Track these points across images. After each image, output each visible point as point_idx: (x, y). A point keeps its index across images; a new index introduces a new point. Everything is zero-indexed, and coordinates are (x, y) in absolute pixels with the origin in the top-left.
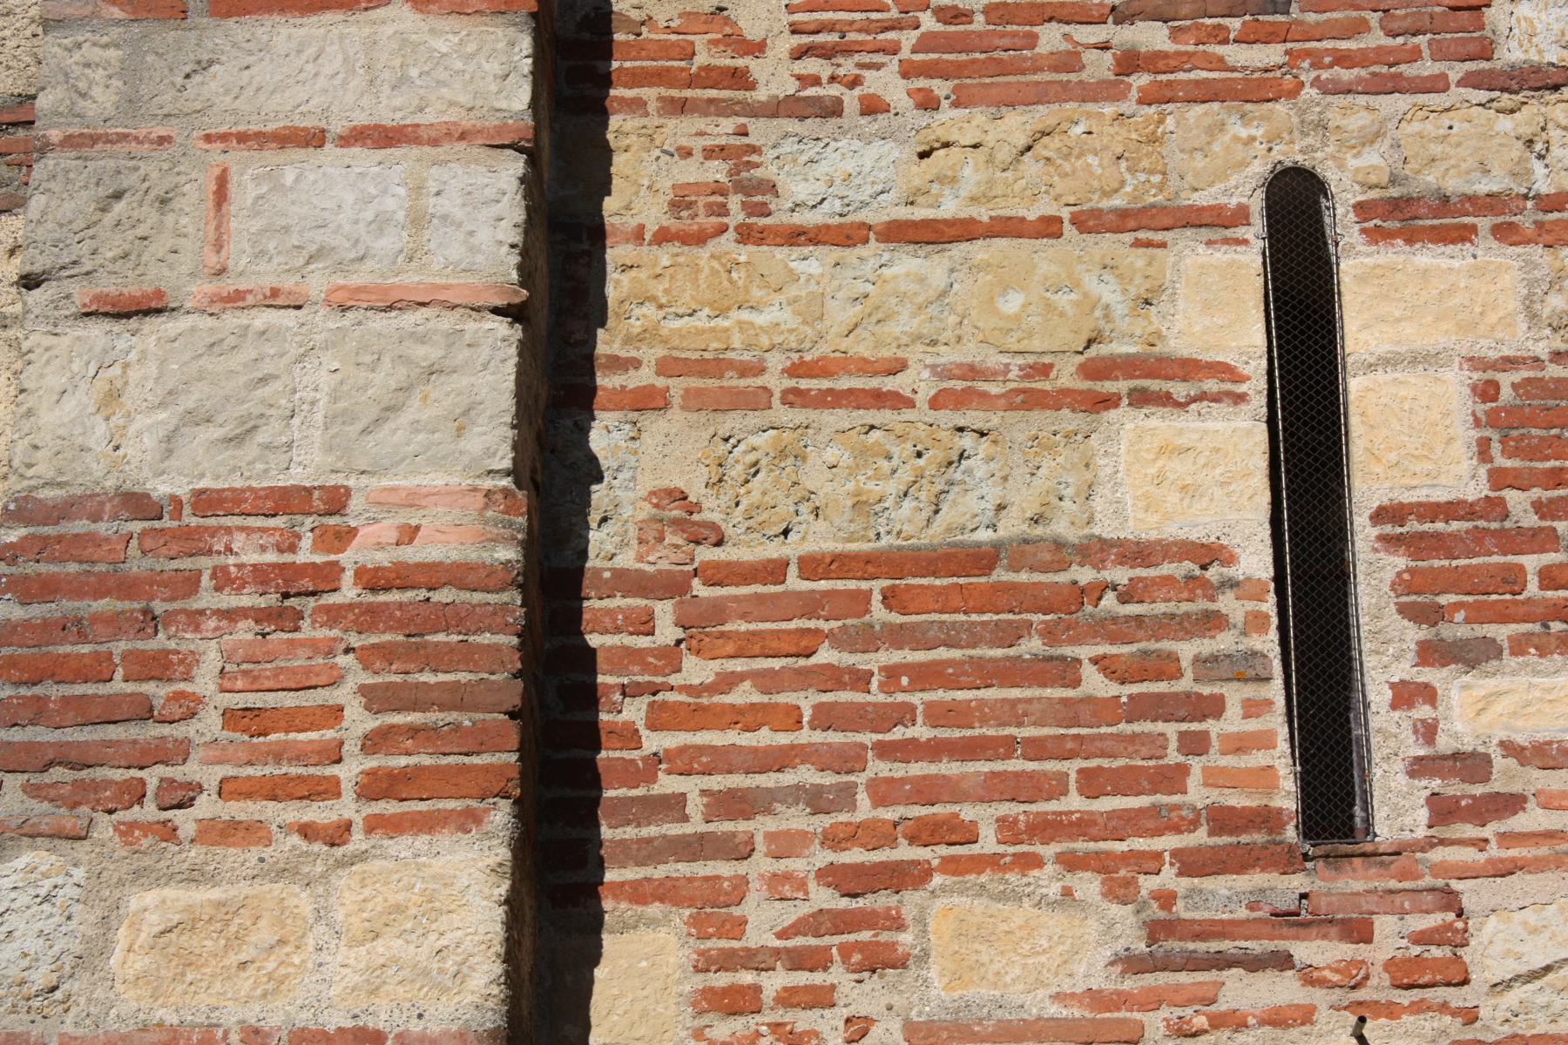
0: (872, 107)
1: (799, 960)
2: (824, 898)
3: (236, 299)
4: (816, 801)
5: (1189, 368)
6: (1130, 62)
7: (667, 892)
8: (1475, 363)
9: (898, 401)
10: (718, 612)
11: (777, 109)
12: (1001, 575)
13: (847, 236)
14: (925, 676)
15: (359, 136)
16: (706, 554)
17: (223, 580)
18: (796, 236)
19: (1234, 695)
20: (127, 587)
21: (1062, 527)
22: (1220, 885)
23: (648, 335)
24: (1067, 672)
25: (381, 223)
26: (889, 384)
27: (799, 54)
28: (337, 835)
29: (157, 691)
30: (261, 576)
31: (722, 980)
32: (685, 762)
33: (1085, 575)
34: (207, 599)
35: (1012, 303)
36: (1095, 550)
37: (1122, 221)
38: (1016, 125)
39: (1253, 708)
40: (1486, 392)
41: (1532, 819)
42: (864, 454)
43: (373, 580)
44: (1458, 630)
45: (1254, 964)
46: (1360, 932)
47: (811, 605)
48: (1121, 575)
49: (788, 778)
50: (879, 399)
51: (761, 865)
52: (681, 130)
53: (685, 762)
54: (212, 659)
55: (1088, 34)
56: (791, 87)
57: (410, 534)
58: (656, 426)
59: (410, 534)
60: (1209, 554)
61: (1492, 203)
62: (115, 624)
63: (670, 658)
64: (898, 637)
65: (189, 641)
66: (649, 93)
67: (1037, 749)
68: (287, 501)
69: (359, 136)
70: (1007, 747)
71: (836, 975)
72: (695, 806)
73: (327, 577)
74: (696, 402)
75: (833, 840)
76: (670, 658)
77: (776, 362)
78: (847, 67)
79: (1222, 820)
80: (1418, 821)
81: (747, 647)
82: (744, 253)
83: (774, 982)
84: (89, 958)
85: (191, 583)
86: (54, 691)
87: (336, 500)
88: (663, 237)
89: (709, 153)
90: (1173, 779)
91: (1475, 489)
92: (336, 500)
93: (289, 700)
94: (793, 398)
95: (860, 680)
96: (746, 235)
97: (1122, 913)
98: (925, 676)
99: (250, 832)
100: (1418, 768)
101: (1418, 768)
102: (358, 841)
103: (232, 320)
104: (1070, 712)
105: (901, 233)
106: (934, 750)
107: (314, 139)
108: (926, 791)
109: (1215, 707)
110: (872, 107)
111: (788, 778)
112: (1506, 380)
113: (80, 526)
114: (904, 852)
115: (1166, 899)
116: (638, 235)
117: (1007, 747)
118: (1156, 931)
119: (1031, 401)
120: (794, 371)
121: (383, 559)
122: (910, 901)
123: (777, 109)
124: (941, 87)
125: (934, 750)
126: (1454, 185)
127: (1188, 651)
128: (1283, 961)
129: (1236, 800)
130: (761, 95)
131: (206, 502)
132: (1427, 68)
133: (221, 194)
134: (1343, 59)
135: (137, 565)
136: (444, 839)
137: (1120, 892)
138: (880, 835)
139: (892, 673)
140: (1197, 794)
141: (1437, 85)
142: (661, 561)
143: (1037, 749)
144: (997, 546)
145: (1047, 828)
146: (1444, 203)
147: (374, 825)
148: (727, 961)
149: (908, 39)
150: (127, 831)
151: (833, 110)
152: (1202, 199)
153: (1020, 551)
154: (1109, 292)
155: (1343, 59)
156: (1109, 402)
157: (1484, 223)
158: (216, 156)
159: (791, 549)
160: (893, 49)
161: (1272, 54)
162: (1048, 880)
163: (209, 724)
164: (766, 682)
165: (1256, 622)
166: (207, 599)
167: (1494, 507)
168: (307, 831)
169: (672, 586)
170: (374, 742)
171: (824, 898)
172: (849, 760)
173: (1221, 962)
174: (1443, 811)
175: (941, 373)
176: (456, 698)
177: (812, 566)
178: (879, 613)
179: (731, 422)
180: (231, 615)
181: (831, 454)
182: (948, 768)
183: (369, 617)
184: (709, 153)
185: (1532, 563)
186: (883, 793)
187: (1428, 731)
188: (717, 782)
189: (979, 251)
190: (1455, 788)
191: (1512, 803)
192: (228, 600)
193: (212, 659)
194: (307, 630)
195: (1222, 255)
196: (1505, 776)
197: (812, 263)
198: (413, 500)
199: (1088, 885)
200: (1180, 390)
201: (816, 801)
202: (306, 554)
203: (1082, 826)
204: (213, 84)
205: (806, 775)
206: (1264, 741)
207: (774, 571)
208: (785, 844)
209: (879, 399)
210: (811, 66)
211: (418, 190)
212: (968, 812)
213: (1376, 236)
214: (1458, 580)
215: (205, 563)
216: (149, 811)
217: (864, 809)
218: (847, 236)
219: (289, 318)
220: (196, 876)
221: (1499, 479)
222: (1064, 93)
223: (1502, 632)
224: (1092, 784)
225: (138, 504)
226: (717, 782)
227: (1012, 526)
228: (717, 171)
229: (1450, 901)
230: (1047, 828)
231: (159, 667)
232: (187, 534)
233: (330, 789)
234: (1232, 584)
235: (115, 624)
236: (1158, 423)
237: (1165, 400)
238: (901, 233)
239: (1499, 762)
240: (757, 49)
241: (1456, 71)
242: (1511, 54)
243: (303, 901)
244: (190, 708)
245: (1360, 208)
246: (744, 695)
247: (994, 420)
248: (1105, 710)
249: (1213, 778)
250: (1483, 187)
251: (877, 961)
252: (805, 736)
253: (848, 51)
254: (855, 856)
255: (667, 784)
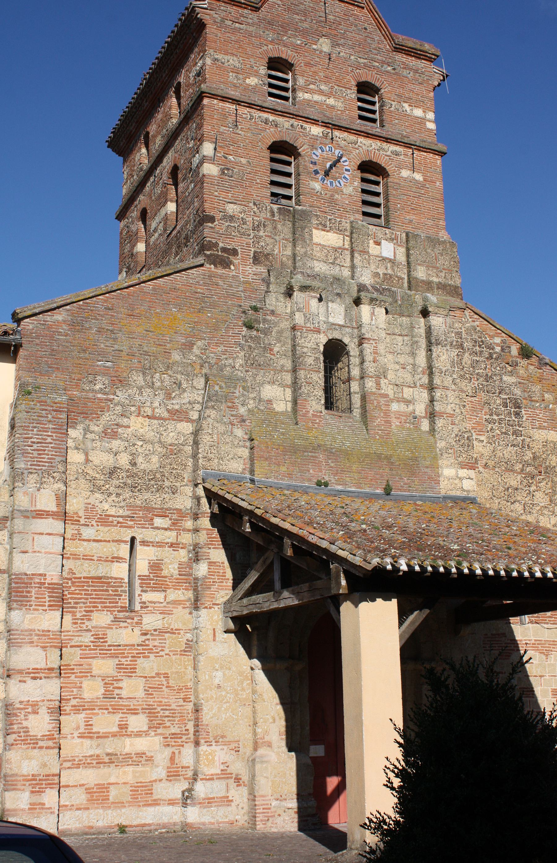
0: (92, 526)
1: (82, 619)
2: (84, 613)
3: (35, 552)
4: (84, 603)
5: (122, 558)
6: (118, 523)
7: (70, 612)
8: (149, 560)
9: (94, 560)
10: (75, 582)
11: (83, 525)
12: (102, 580)
13: (89, 541)
14: (95, 590)
15: (47, 534)
16: (74, 576)
17: (34, 583)
18: (84, 540)
19: (124, 594)
20: (25, 583)
21: (108, 575)
22: (121, 614)
23: (69, 550)
24: (108, 591)
25: (49, 544)
26: (92, 558)
27: (85, 518)
28: (46, 610)
29: (28, 595)
30: (38, 583)
31: (74, 621)
32: (71, 598)
33: (110, 580)
34: (33, 585)
35: (105, 550)
36: (111, 578)
37: (117, 541)
38: (107, 529)
39: (125, 596)
40: (150, 563)
41: (149, 609)
42: (90, 565)
43: (49, 584)
44: (145, 589)
45: (123, 622)
46: (133, 619)
47: (84, 582)
48: (114, 581)
49: (81, 601)
50: (91, 560)
51: (78, 609)
52: (73, 526)
53: (71, 598)
54: (33, 592)
55: (114, 519)
56: (84, 523)
57: (52, 579)
58: (69, 561)
59: (52, 579)
60: (122, 579)
61: (152, 542)
62: (24, 587)
63: (70, 587)
64: (92, 586)
65: (31, 590)
66: (70, 522)
67: (105, 599)
68: (41, 575)
69: (47, 534)
70: (101, 598)
71: (85, 621)
72: (72, 603)
73: (44, 583)
74: (73, 558)
75: (85, 607)
76: (70, 587)
77: (81, 555)
78: (90, 521)
79: (122, 607)
80: (139, 608)
81: (78, 586)
82: (79, 542)
83: (79, 621)
84: (23, 622)
85: (31, 583)
86: (19, 594)
87: (45, 575)
88: (71, 539)
89: (76, 530)
90: (117, 603)
91: (148, 574)
92: (45, 575)
93: (41, 596)
94: (83, 559)
95: (88, 591)
96: (79, 540)
97: (112, 616)
98: (95, 590)
99: (38, 610)
100: (140, 603)
101: (140, 603)
102: (48, 611)
103: (35, 554)
104: (108, 595)
105: (94, 541)
106: (95, 598)
107: (42, 534)
108: (94, 603)
109: (121, 595)
110: (92, 526)
111: (81, 601)
112: (152, 562)
113: (20, 576)
114: (92, 609)
115: (116, 615)
116: (68, 539)
117: (101, 598)
118: (115, 618)
119: (107, 561)
120: (83, 556)
121: (50, 582)
122: (92, 614)
123: (83, 525)
124: (99, 524)
125: (95, 598)
126: (148, 540)
127: (119, 589)
128: (126, 622)
129: (123, 605)
130: (81, 523)
131: (33, 575)
132: (147, 526)
133: (33, 540)
134: (139, 524)
135: (26, 581)
136: (56, 611)
137: (112, 614)
138: (89, 607)
139: (92, 590)
140: (119, 604)
141: (148, 528)
142: (69, 577)
143: (105, 599)
144: (102, 576)
145: (105, 607)
146: (147, 542)
147: (49, 610)
148: (75, 619)
149: (96, 518)
150: (26, 609)
151: (88, 525)
152: (124, 539)
153: (105, 577)
154: (114, 549)
155: (139, 524)
156: (114, 562)
157: (151, 544)
158: (33, 535)
159: (82, 575)
160: (95, 519)
161: (132, 523)
162: (105, 613)
163: (33, 599)
164: (80, 590)
165: (126, 587)
166: (33, 585)
167: (149, 576)
168: (43, 610)
169: (70, 579)
170: (49, 601)
171: (84, 613)
172: (87, 599)
173: (120, 621)
174: (142, 607)
175: (98, 557)
176: (57, 597)
177: (84, 578)
178: (90, 583)
179: (77, 561)
180: (35, 587)
181: (86, 565)
182: (96, 600)
183: (49, 588)
184: (76, 530)
185: (152, 582)
186: (90, 603)
187: (141, 599)
188: (75, 601)
189: (102, 543)
190: (143, 605)
191: (147, 607)
192: (35, 585)
193: (33, 592)
194: (43, 589)
195: (126, 546)
196: (148, 604)
197: (85, 543)
198: (52, 575)
199: (109, 613)
200: (121, 561)
201: (84, 603)
202: (42, 581)
203: (109, 607)
204: (32, 527)
205: (83, 600)
206: (126, 599)
207: (80, 578)
208: (81, 607)
209: (91, 560)
210: (86, 520)
211: (53, 541)
212: (98, 605)
213: (141, 545)
214: (145, 583)
215: (33, 581)
216: (28, 607)
217: (88, 604)
218: (89, 541)
219: (40, 554)
220: (33, 614)
221: (150, 573)
222: (112, 526)
223: (149, 589)
224: (110, 603)
225: (26, 574)
226: (75, 601)
227: (103, 574)
228: (76, 532)
229: (141, 616)
230: (105, 607)
231: (28, 592)
232: (31, 578)
233: (45, 606)
234: (124, 582)
235: (24, 587)
236: (118, 564)
237: (119, 562)
238: (94, 541)
239: (147, 603)
240: (81, 517)
241: (150, 527)
242: (155, 525)
243: (42, 617)
244: (31, 596)
245: (140, 542)
246: (77, 592)
247: (103, 563)
248: (111, 595)
249: (121, 603)
250: (151, 540)
251: (89, 620)
252: (83, 596)
253: (90, 518)
254: (87, 609)
255: (70, 601)
